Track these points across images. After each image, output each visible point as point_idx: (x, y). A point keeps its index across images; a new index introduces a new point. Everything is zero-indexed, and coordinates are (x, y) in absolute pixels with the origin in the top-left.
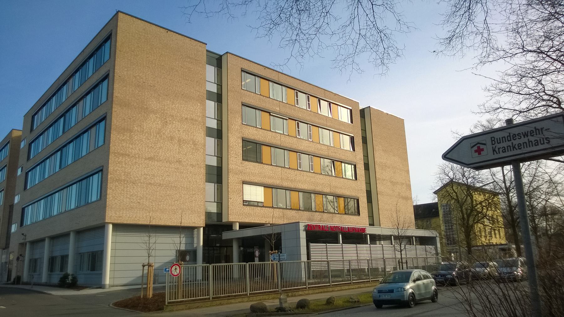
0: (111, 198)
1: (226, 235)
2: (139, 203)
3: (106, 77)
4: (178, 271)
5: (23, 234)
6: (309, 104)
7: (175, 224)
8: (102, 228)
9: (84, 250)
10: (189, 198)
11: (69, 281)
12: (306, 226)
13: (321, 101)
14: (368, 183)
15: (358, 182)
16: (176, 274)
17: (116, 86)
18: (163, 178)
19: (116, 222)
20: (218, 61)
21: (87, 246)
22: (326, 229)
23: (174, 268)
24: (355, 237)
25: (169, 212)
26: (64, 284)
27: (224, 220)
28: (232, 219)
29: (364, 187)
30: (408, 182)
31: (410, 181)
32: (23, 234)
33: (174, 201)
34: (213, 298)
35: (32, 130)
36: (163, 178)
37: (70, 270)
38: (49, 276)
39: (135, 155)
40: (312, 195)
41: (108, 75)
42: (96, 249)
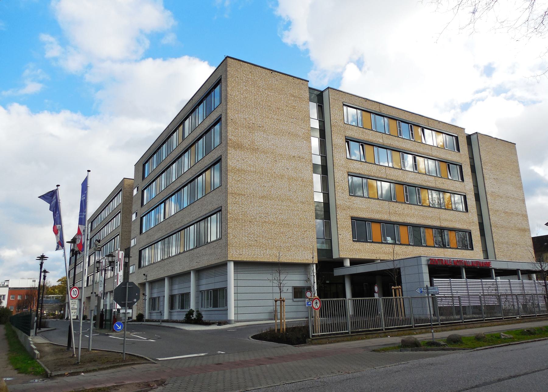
0: (232, 237)
1: (338, 272)
2: (256, 240)
3: (218, 121)
4: (318, 305)
5: (144, 275)
6: (412, 134)
7: (290, 261)
8: (224, 265)
9: (203, 288)
10: (301, 235)
11: (194, 316)
12: (428, 260)
13: (425, 130)
14: (480, 215)
15: (469, 214)
16: (316, 308)
17: (230, 129)
18: (277, 216)
19: (237, 259)
20: (319, 97)
21: (209, 283)
22: (449, 263)
23: (315, 302)
24: (480, 271)
25: (284, 249)
26: (189, 320)
27: (335, 256)
28: (342, 256)
29: (476, 219)
30: (524, 213)
31: (526, 211)
32: (144, 275)
33: (288, 238)
34: (352, 333)
35: (143, 178)
36: (277, 216)
37: (193, 306)
38: (170, 313)
39: (250, 194)
40: (422, 229)
41: (221, 118)
42: (185, 291)
